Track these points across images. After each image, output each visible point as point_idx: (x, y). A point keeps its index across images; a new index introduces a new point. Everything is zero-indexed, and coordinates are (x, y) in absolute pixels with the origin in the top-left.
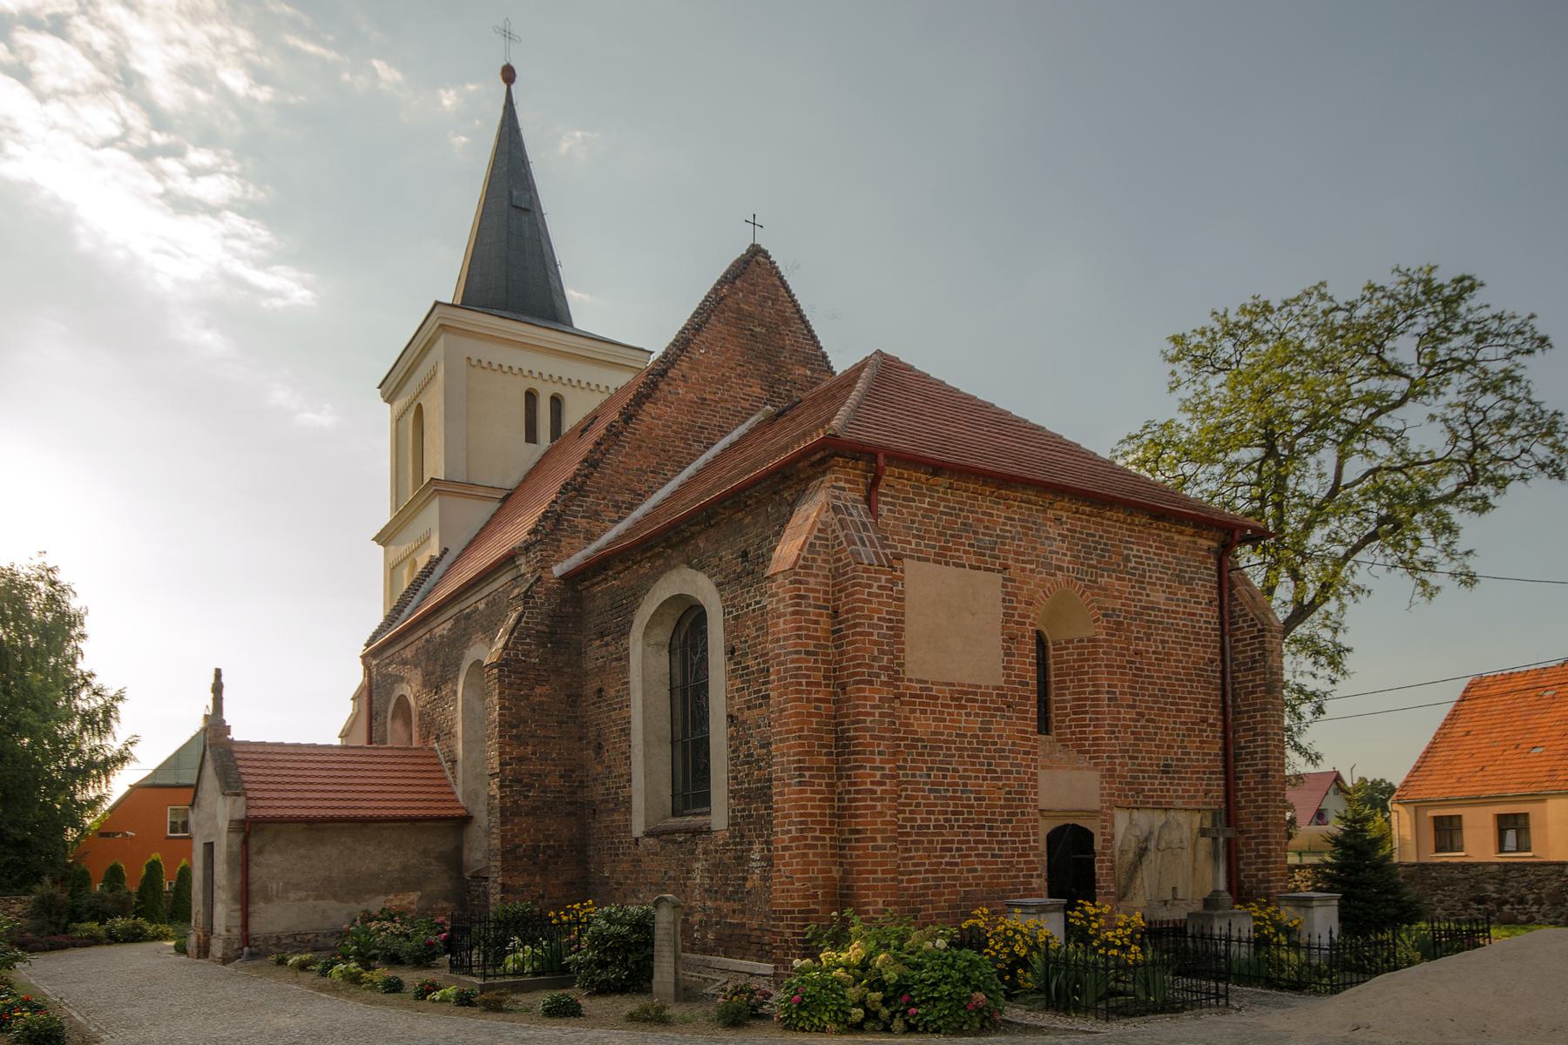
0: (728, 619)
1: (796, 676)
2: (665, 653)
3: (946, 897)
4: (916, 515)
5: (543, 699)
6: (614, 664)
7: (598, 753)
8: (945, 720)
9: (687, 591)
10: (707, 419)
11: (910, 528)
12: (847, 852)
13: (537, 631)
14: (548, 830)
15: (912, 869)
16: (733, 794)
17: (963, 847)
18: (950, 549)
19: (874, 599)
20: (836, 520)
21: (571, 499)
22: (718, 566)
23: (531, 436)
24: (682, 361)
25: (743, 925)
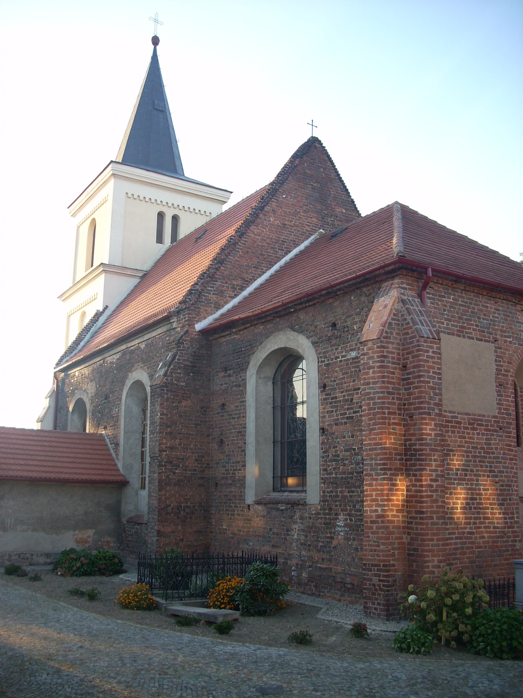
0: (321, 366)
1: (382, 408)
2: (270, 383)
3: (468, 555)
4: (446, 306)
5: (187, 409)
6: (235, 388)
7: (221, 446)
8: (465, 438)
9: (291, 345)
10: (286, 236)
11: (443, 314)
12: (413, 525)
13: (185, 365)
14: (187, 495)
15: (448, 536)
16: (324, 480)
17: (477, 521)
18: (464, 328)
19: (430, 360)
20: (404, 309)
21: (207, 282)
22: (314, 331)
23: (160, 239)
24: (272, 202)
25: (331, 569)
